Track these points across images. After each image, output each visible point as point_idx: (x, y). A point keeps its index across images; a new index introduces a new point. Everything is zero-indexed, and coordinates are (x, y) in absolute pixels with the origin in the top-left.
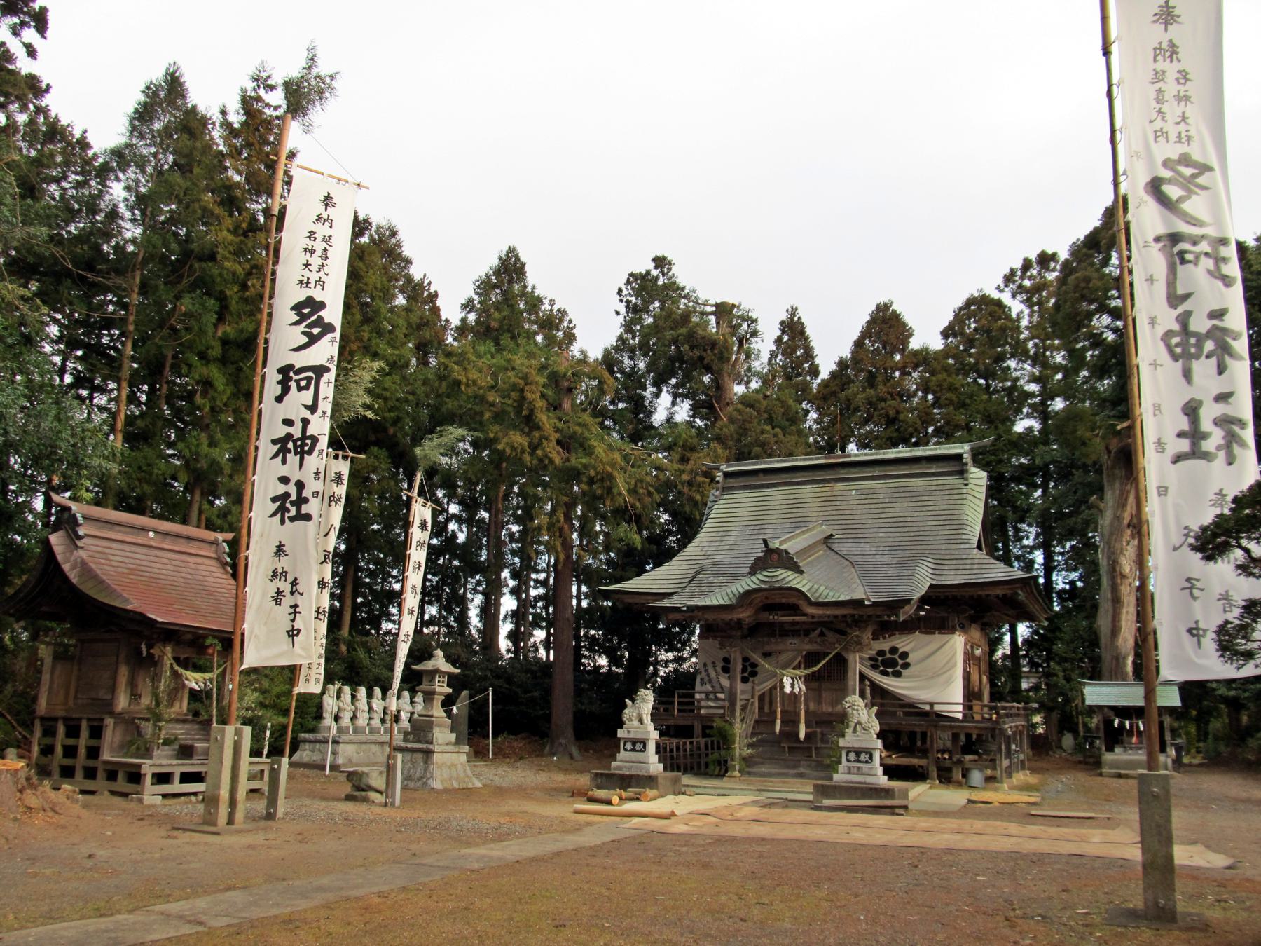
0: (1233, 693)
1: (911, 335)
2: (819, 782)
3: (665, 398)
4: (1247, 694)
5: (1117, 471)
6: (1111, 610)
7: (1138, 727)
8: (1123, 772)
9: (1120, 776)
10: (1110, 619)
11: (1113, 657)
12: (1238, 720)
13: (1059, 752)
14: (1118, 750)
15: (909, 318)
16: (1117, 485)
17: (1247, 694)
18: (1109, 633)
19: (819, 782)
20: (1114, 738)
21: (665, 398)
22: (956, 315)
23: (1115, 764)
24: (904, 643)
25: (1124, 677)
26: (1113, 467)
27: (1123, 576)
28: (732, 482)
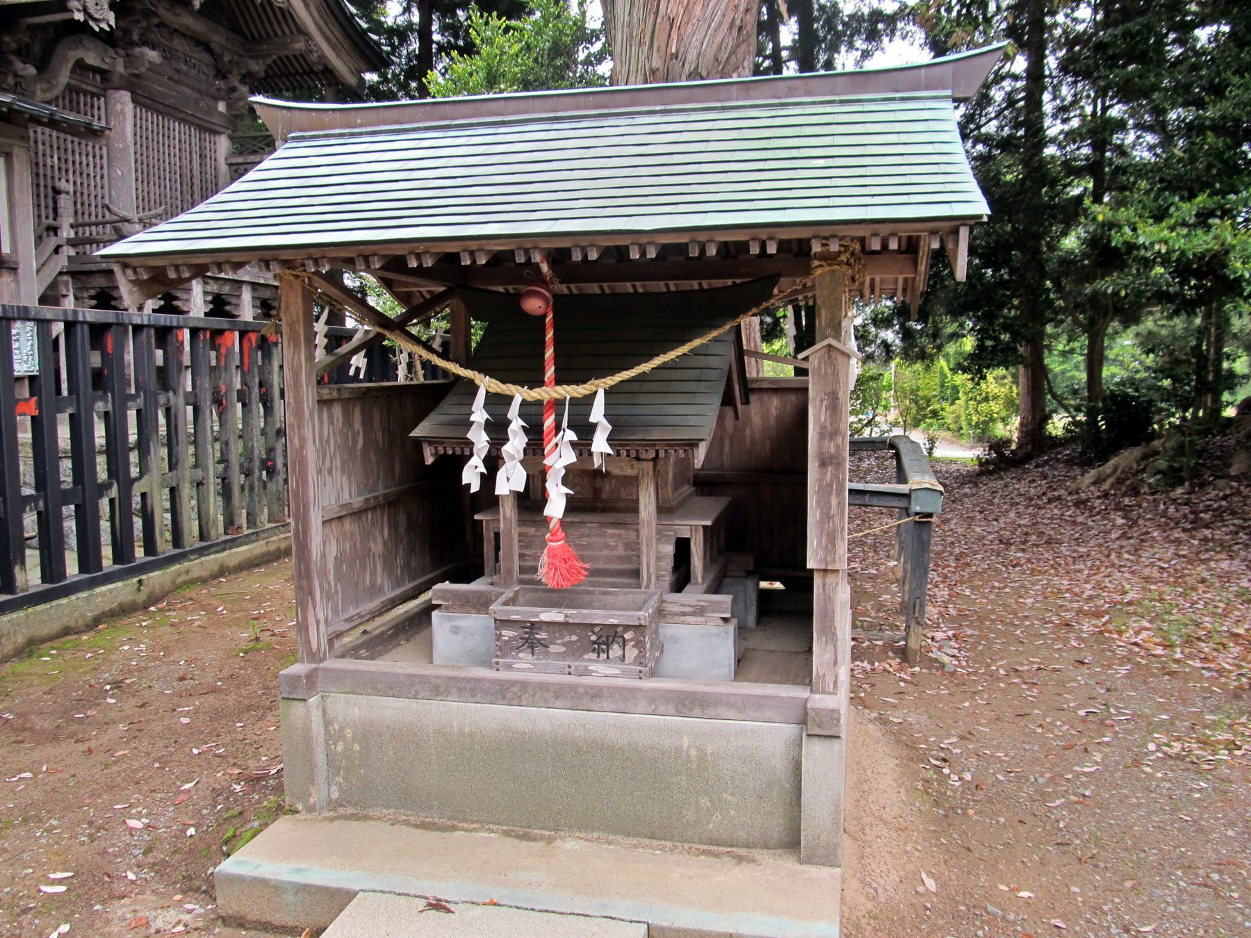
14: (457, 632)
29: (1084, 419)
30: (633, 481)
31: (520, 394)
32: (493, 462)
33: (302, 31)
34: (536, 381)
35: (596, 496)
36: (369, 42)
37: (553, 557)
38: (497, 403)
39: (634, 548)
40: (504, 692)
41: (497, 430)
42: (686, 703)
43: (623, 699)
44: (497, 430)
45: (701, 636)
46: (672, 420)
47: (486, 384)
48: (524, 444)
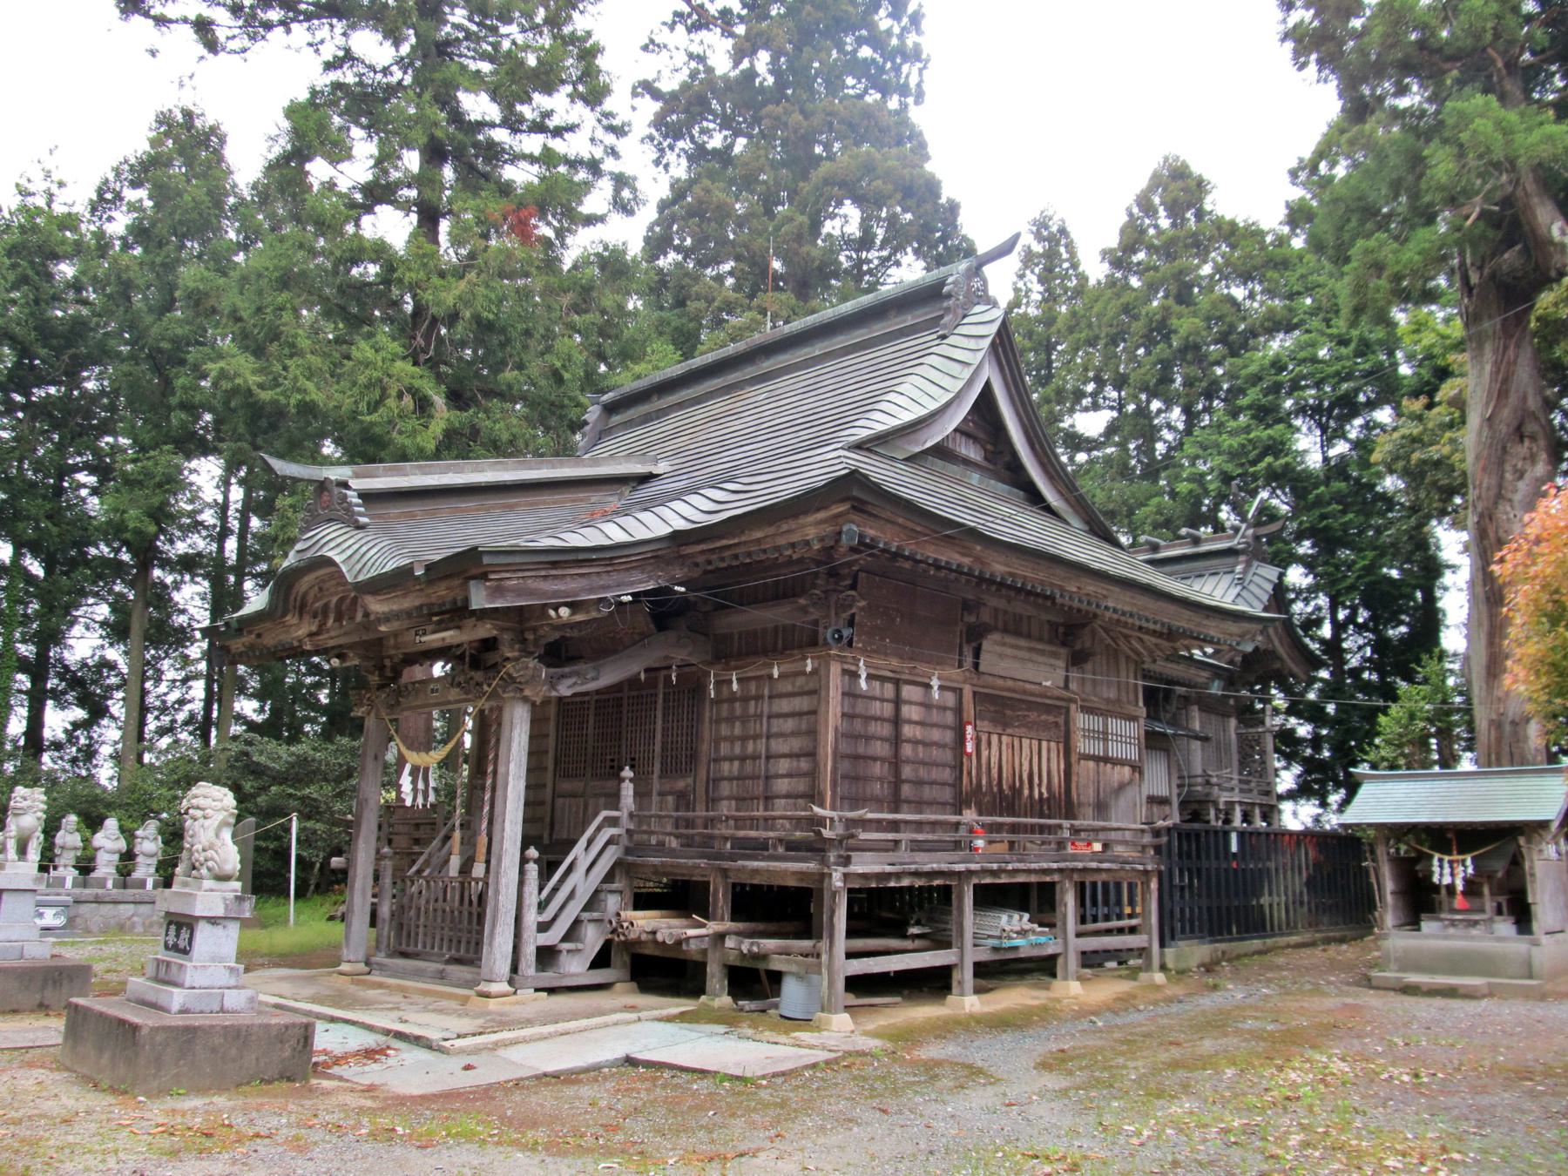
8: (1413, 978)
14: (1428, 926)
18: (1483, 672)
28: (616, 419)
29: (6, 766)
30: (1481, 885)
31: (1447, 858)
32: (1441, 875)
33: (1279, 658)
34: (1450, 854)
35: (1472, 888)
36: (1295, 633)
37: (1458, 902)
38: (1441, 860)
39: (1483, 905)
40: (1446, 938)
41: (1441, 867)
42: (1500, 939)
43: (1480, 938)
44: (1441, 867)
45: (1505, 927)
46: (995, 772)
47: (1437, 856)
48: (1449, 871)
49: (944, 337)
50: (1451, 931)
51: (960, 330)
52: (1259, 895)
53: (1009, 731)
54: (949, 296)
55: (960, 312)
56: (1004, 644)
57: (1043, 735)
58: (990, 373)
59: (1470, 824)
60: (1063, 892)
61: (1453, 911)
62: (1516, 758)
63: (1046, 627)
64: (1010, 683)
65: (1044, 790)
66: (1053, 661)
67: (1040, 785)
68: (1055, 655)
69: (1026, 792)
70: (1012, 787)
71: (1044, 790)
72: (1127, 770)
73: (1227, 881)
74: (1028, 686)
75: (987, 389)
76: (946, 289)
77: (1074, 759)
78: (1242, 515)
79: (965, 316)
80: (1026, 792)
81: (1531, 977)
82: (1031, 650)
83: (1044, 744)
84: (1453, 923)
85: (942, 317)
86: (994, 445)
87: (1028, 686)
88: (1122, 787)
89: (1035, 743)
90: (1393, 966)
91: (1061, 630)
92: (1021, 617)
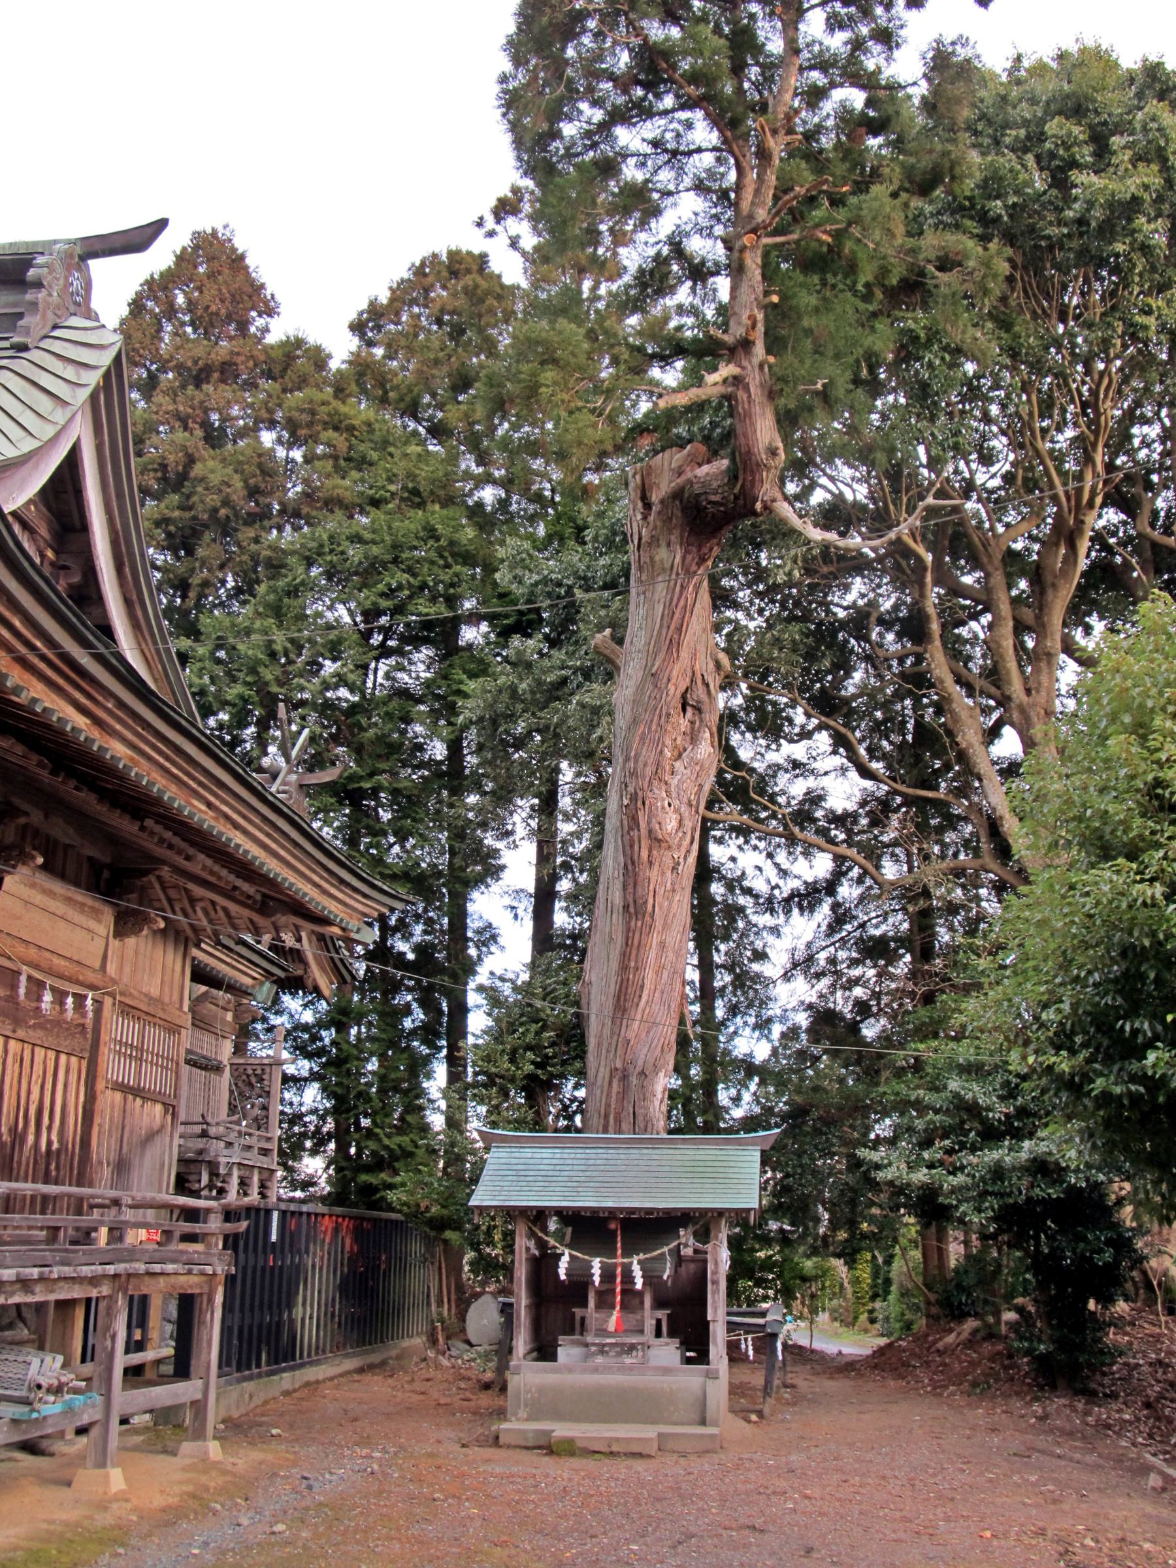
0: (921, 1176)
1: (330, 356)
2: (930, 794)
3: (603, 375)
4: (960, 1179)
5: (662, 554)
6: (619, 940)
7: (628, 1278)
8: (561, 1430)
9: (550, 1448)
10: (615, 965)
11: (614, 1070)
12: (942, 1253)
13: (458, 1346)
15: (266, 266)
16: (661, 589)
17: (960, 1179)
18: (610, 1004)
19: (930, 794)
20: (557, 1311)
21: (603, 375)
22: (419, 271)
23: (549, 1405)
24: (473, 924)
25: (639, 1123)
26: (654, 541)
27: (656, 841)
45: (667, 1352)
49: (24, 348)
50: (600, 1360)
51: (45, 344)
52: (290, 1306)
53: (21, 1033)
54: (38, 285)
55: (51, 319)
56: (33, 886)
57: (65, 1044)
58: (82, 431)
59: (650, 1211)
60: (110, 1314)
61: (603, 1332)
62: (640, 1122)
63: (85, 866)
64: (32, 952)
65: (54, 1137)
66: (92, 924)
67: (50, 1128)
68: (96, 914)
69: (31, 1138)
70: (13, 1130)
71: (54, 1137)
72: (159, 1108)
73: (254, 1279)
74: (57, 961)
75: (72, 461)
76: (32, 273)
77: (100, 1085)
78: (287, 756)
79: (55, 327)
80: (31, 1138)
81: (703, 1422)
82: (69, 900)
83: (63, 1058)
84: (602, 1350)
85: (21, 316)
86: (57, 552)
87: (57, 961)
88: (151, 1136)
89: (51, 1055)
90: (522, 1413)
91: (106, 874)
92: (56, 842)
